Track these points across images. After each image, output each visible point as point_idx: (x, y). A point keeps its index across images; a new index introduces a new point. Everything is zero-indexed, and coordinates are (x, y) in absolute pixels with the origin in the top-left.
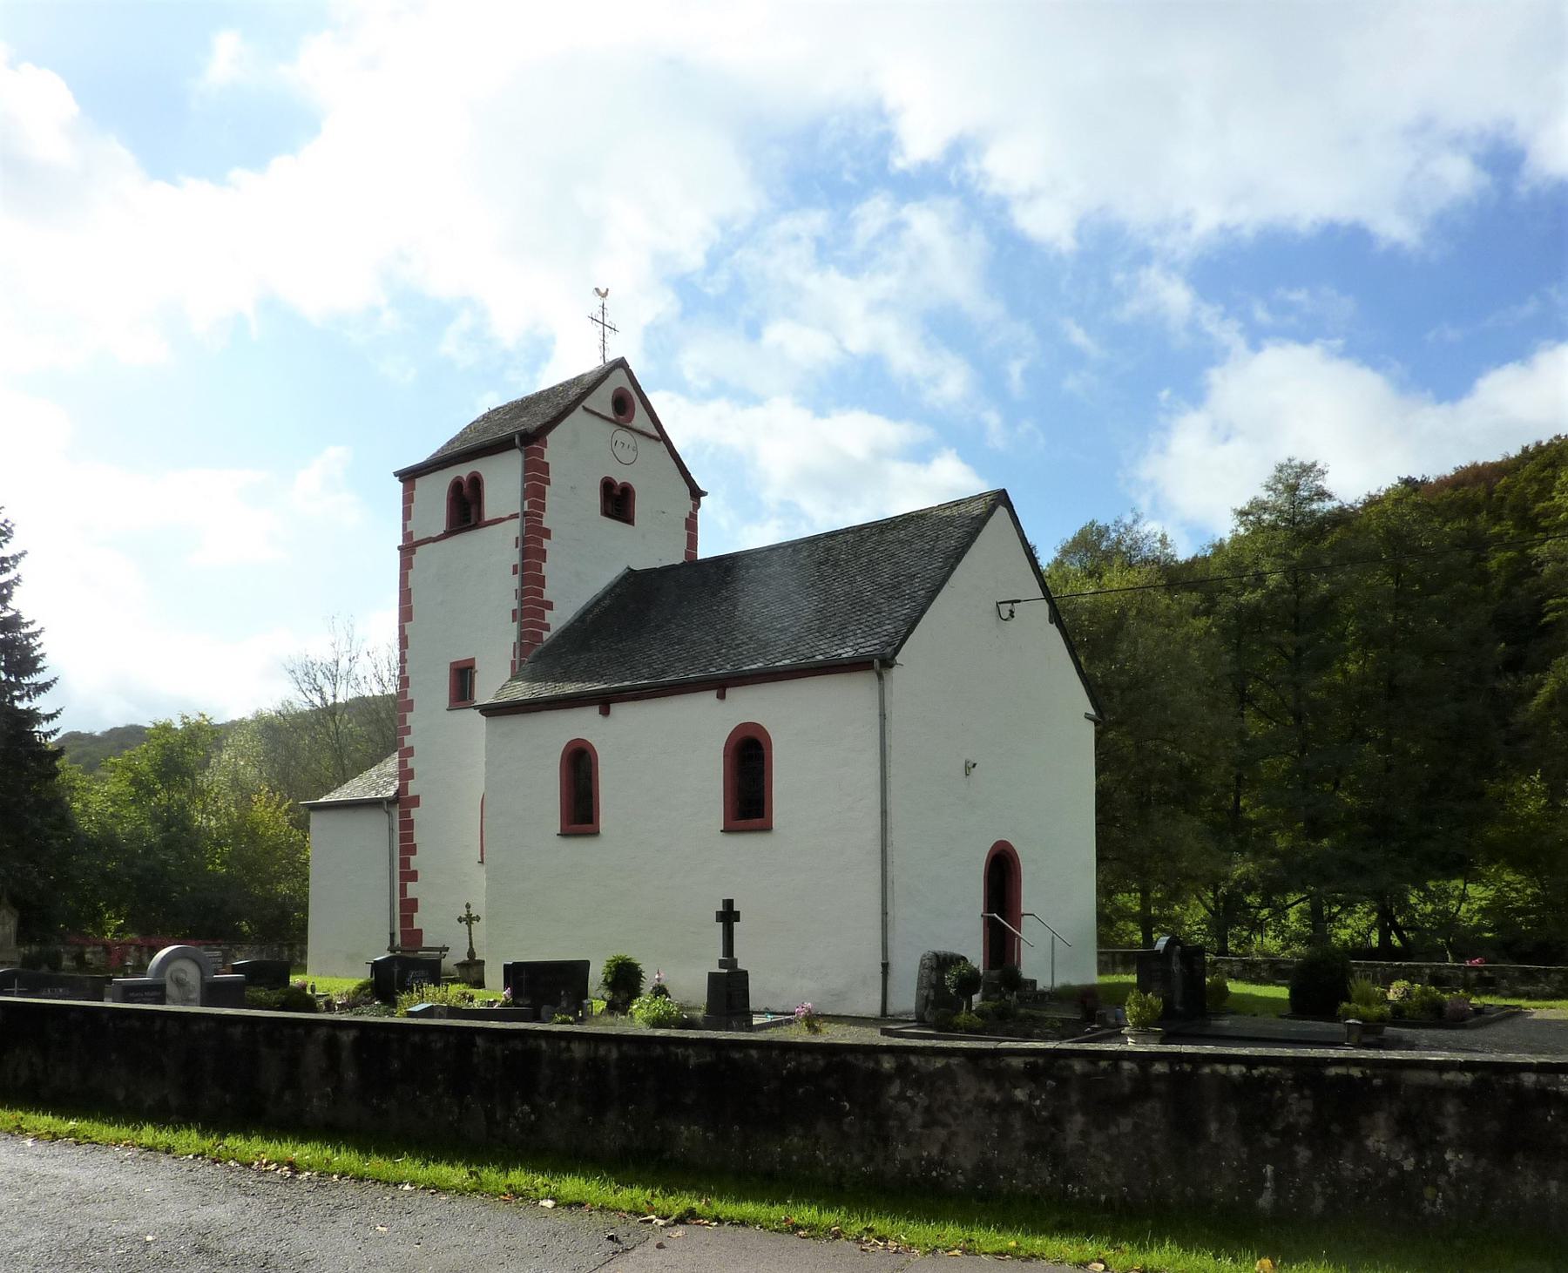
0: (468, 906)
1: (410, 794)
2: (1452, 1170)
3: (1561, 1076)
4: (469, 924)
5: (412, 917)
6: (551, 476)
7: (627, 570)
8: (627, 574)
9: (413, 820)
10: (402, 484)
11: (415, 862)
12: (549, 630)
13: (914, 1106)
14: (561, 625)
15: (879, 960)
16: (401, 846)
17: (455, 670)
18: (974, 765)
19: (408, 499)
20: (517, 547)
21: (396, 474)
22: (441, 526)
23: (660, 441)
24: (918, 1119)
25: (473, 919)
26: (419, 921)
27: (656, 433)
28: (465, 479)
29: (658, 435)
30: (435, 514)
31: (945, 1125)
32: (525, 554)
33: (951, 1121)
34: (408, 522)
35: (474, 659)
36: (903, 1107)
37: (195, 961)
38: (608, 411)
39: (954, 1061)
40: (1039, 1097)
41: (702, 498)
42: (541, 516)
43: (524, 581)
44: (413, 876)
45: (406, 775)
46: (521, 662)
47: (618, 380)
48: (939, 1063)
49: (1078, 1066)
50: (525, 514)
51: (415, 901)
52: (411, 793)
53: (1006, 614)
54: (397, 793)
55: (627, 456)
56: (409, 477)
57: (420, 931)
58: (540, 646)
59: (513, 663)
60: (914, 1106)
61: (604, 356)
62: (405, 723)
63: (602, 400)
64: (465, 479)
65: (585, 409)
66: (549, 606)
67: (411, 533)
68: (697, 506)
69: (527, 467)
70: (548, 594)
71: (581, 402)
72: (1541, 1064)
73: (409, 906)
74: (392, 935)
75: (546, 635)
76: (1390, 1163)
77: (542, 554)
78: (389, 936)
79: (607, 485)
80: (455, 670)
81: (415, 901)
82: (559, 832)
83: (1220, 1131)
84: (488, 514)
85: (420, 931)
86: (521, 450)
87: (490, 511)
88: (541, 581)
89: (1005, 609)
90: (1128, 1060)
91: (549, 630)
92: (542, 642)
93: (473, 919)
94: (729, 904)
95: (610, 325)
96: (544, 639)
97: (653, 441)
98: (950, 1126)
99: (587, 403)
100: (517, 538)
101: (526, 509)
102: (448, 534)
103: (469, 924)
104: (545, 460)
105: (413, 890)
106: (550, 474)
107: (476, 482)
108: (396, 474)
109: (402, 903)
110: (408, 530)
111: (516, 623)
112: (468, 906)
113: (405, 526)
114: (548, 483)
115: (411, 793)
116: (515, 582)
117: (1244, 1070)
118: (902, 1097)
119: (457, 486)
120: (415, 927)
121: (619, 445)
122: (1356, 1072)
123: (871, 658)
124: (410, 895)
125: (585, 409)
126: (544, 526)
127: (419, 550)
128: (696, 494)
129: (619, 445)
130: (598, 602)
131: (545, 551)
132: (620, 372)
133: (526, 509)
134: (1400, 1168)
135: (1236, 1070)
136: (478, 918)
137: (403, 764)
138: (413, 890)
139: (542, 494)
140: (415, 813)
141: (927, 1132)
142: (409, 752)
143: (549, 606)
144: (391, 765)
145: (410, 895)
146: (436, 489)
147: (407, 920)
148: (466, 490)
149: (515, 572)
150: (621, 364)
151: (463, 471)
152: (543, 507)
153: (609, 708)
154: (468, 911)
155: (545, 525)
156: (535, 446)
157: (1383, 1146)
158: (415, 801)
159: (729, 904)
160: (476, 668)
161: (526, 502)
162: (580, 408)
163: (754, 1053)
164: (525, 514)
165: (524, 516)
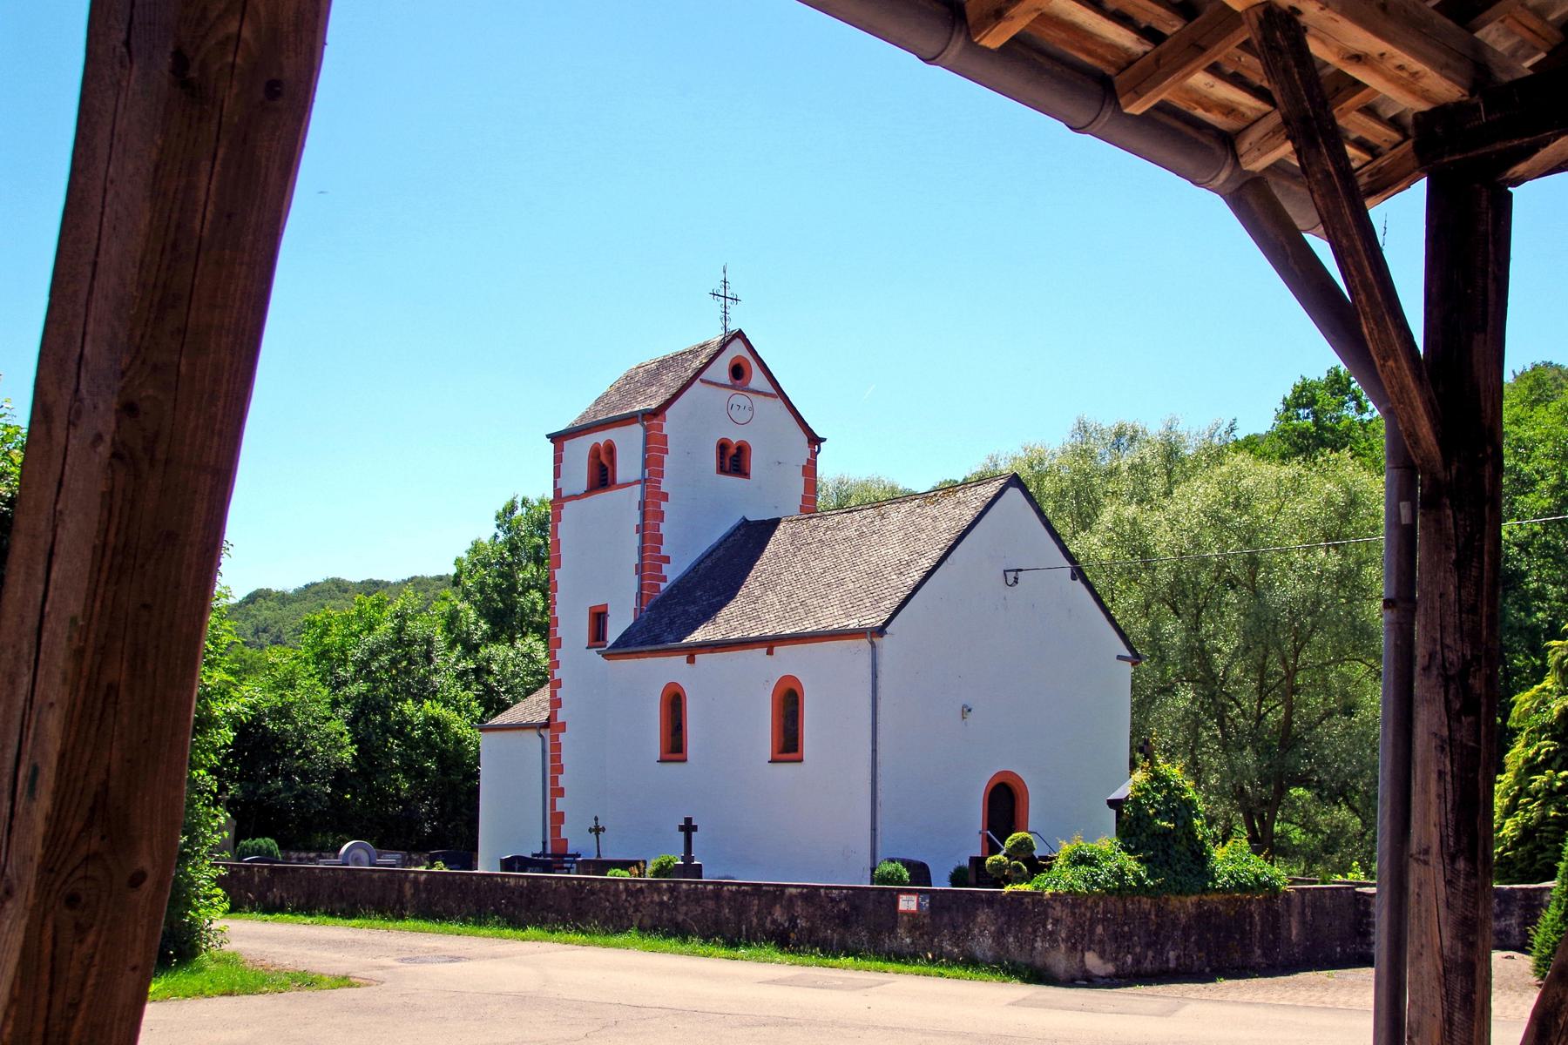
0: (596, 819)
1: (559, 720)
6: (669, 447)
8: (742, 524)
17: (594, 614)
18: (970, 710)
19: (558, 460)
21: (548, 436)
24: (632, 910)
25: (600, 830)
26: (565, 832)
27: (769, 388)
29: (774, 392)
30: (579, 477)
36: (627, 904)
37: (366, 851)
38: (725, 377)
41: (822, 444)
42: (659, 482)
44: (560, 792)
45: (556, 703)
47: (737, 349)
51: (562, 814)
53: (1011, 581)
55: (742, 416)
56: (557, 439)
63: (721, 370)
66: (667, 560)
68: (815, 455)
69: (647, 440)
70: (664, 551)
73: (559, 818)
75: (663, 586)
76: (782, 924)
77: (660, 516)
79: (723, 447)
80: (594, 614)
81: (562, 814)
84: (620, 478)
86: (643, 425)
87: (621, 477)
88: (659, 539)
89: (1011, 576)
93: (600, 830)
94: (688, 820)
96: (662, 589)
99: (704, 376)
101: (647, 476)
105: (561, 804)
107: (610, 449)
108: (548, 436)
112: (596, 819)
119: (595, 453)
124: (558, 809)
127: (567, 505)
128: (815, 440)
129: (735, 407)
130: (709, 554)
132: (738, 343)
135: (734, 888)
136: (603, 830)
137: (553, 694)
138: (561, 804)
139: (661, 463)
140: (562, 737)
142: (558, 684)
144: (545, 692)
145: (558, 809)
146: (580, 450)
147: (556, 830)
148: (603, 459)
150: (740, 335)
151: (600, 438)
152: (661, 474)
158: (563, 726)
159: (688, 820)
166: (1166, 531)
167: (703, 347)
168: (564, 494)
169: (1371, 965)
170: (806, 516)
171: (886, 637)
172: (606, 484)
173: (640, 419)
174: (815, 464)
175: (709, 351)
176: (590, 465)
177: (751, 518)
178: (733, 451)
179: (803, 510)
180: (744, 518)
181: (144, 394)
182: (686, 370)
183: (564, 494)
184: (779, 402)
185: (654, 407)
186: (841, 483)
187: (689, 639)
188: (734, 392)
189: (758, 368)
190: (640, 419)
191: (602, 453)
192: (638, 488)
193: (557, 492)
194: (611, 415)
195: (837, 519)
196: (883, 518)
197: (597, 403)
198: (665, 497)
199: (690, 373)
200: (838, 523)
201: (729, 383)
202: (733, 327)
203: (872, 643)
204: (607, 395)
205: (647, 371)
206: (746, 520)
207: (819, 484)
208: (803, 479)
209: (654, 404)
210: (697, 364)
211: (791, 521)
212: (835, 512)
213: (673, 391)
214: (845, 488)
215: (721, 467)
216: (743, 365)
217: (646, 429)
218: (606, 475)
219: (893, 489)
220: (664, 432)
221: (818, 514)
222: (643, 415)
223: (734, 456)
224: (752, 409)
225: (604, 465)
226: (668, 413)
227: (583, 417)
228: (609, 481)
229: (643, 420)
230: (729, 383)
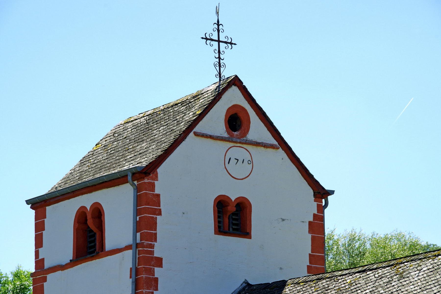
6: (163, 207)
7: (244, 285)
8: (244, 289)
10: (34, 211)
15: (45, 233)
16: (155, 230)
20: (131, 277)
21: (28, 202)
23: (278, 148)
27: (271, 140)
28: (88, 208)
29: (275, 142)
34: (40, 250)
41: (330, 198)
42: (152, 246)
50: (137, 245)
61: (220, 74)
64: (88, 209)
68: (321, 209)
69: (138, 200)
71: (193, 129)
84: (109, 245)
86: (133, 185)
95: (226, 40)
99: (197, 129)
100: (131, 269)
101: (138, 241)
102: (73, 263)
108: (28, 202)
110: (40, 257)
113: (37, 254)
114: (160, 214)
125: (196, 134)
126: (155, 255)
127: (49, 277)
129: (233, 161)
131: (156, 280)
132: (234, 90)
139: (153, 225)
148: (90, 222)
152: (154, 237)
155: (156, 255)
156: (146, 181)
161: (138, 234)
162: (192, 134)
164: (137, 245)
166: (396, 248)
167: (196, 97)
168: (47, 265)
169: (132, 249)
170: (315, 277)
172: (93, 252)
173: (130, 178)
174: (322, 219)
175: (203, 101)
176: (77, 231)
177: (252, 282)
178: (232, 209)
179: (310, 270)
180: (246, 282)
181: (146, 234)
182: (178, 124)
183: (47, 265)
184: (281, 153)
185: (144, 164)
186: (352, 239)
187: (89, 211)
188: (232, 144)
189: (257, 118)
190: (130, 178)
191: (89, 217)
192: (129, 253)
193: (39, 263)
194: (98, 176)
195: (349, 279)
196: (402, 277)
197: (82, 162)
198: (159, 262)
199: (183, 127)
200: (351, 284)
201: (226, 135)
202: (228, 73)
203: (128, 247)
204: (92, 154)
205: (136, 127)
206: (248, 285)
207: (328, 243)
208: (310, 236)
209: (144, 162)
210: (190, 116)
211: (298, 283)
212: (347, 272)
213: (165, 146)
214: (357, 245)
215: (219, 227)
216: (241, 115)
217: (138, 189)
218: (94, 241)
219: (414, 245)
220: (157, 192)
221: (328, 275)
222: (133, 174)
223: (233, 214)
224: (251, 162)
225: (91, 231)
226: (160, 170)
227: (66, 179)
228: (97, 247)
229: (133, 180)
230: (226, 135)
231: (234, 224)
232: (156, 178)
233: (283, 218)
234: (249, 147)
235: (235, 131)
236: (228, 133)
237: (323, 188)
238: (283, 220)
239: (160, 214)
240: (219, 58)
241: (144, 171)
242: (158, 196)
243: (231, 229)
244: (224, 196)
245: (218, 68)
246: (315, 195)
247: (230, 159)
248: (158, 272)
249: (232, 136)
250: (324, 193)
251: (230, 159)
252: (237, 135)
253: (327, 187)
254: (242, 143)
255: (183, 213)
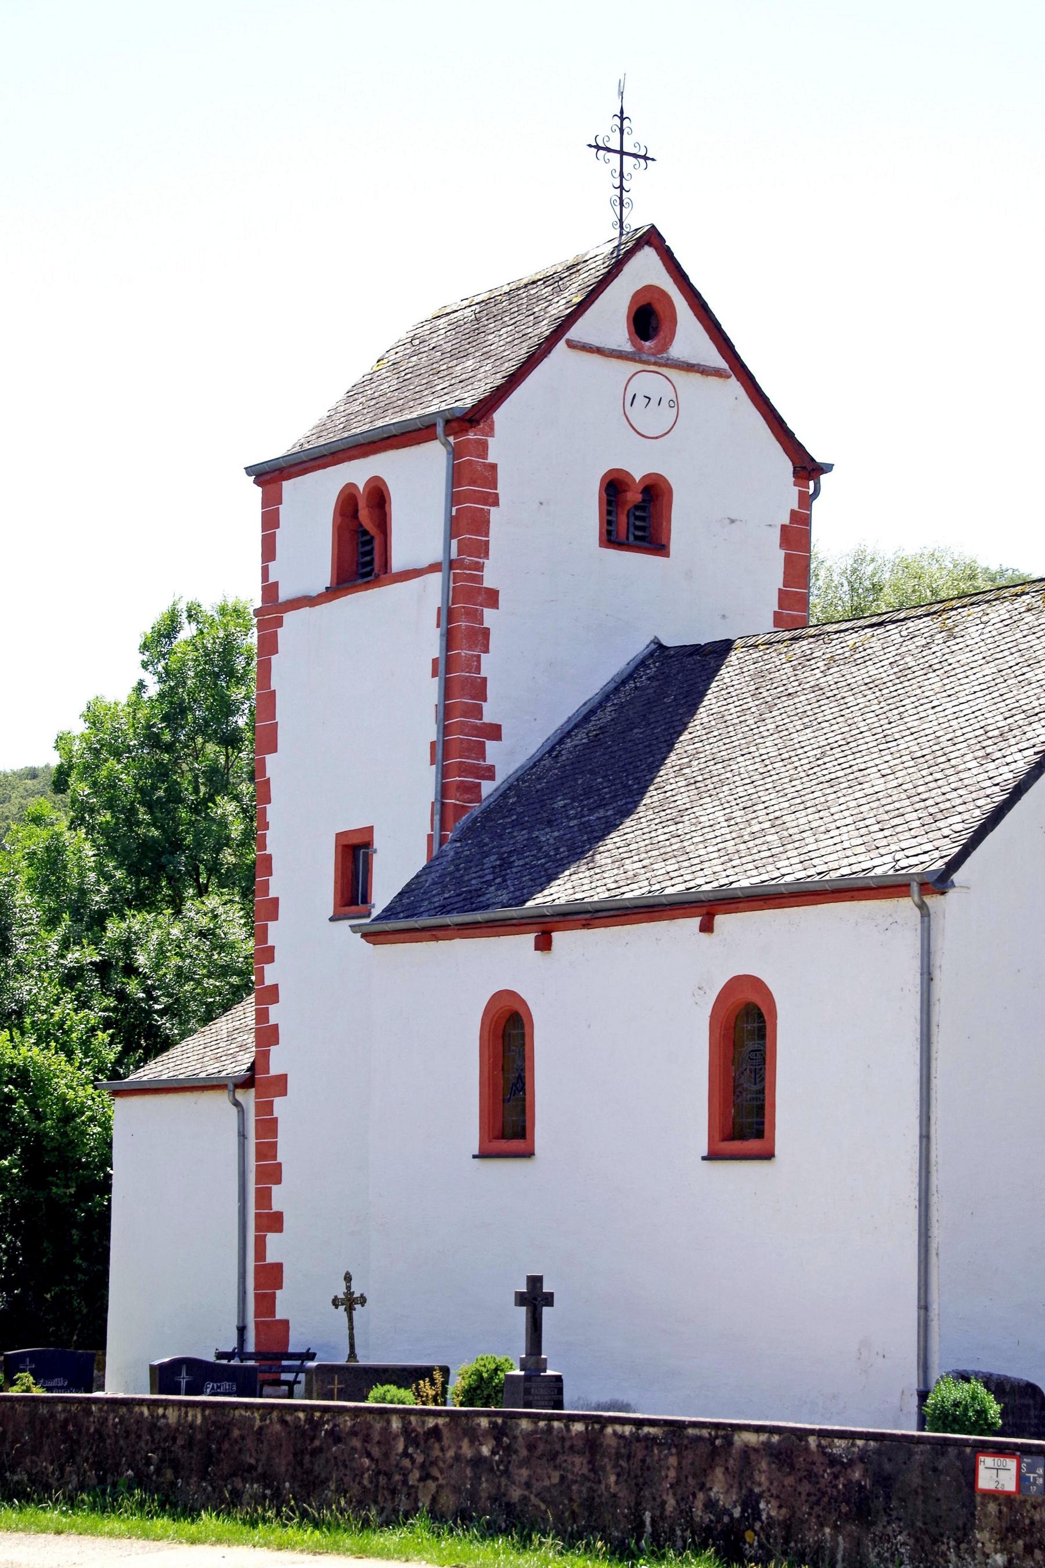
0: (348, 1278)
2: (764, 1517)
3: (836, 1440)
4: (349, 1293)
5: (273, 1297)
6: (500, 490)
7: (653, 646)
9: (280, 1164)
10: (260, 489)
11: (280, 1198)
12: (492, 777)
13: (413, 1461)
14: (517, 765)
20: (438, 626)
21: (249, 470)
22: (322, 577)
23: (729, 377)
24: (416, 1474)
31: (435, 1479)
32: (449, 639)
33: (438, 1475)
34: (271, 564)
35: (370, 829)
38: (620, 336)
39: (441, 1421)
40: (498, 1453)
42: (480, 567)
43: (447, 690)
46: (443, 840)
48: (431, 1422)
49: (525, 1424)
50: (452, 564)
51: (279, 1267)
52: (275, 1070)
54: (252, 1068)
57: (286, 1323)
58: (476, 808)
59: (430, 837)
60: (413, 1461)
62: (266, 942)
65: (571, 345)
66: (494, 732)
67: (276, 585)
69: (457, 475)
70: (490, 713)
71: (564, 334)
72: (821, 1430)
74: (242, 1330)
75: (487, 788)
77: (481, 638)
78: (236, 1332)
82: (476, 1152)
83: (617, 1483)
84: (398, 561)
85: (286, 1323)
87: (400, 558)
88: (479, 689)
90: (558, 1420)
91: (492, 777)
92: (478, 799)
94: (535, 1281)
97: (713, 380)
98: (437, 1479)
99: (574, 333)
101: (454, 555)
102: (333, 592)
103: (349, 1293)
104: (491, 459)
105: (276, 1247)
106: (499, 486)
108: (249, 470)
109: (257, 1269)
110: (271, 580)
111: (434, 766)
112: (348, 1278)
114: (496, 503)
115: (275, 1070)
116: (431, 690)
117: (634, 1430)
118: (405, 1454)
120: (278, 1317)
121: (640, 401)
122: (705, 1433)
123: (904, 881)
125: (571, 345)
129: (640, 401)
131: (486, 632)
132: (648, 256)
133: (454, 555)
134: (731, 1515)
135: (628, 1430)
137: (262, 1015)
138: (276, 1247)
139: (482, 524)
140: (280, 1105)
141: (421, 1484)
142: (271, 994)
143: (494, 732)
147: (266, 1303)
149: (435, 674)
152: (483, 550)
153: (550, 937)
154: (349, 1288)
155: (487, 583)
157: (722, 1497)
159: (535, 1281)
160: (376, 844)
161: (454, 543)
162: (562, 344)
163: (301, 1415)
164: (452, 564)
165: (451, 568)
171: (952, 894)
184: (734, 386)
188: (639, 367)
201: (628, 347)
208: (782, 554)
224: (674, 403)
226: (500, 416)
230: (628, 347)
231: (637, 528)
232: (490, 431)
233: (733, 517)
234: (672, 373)
235: (646, 340)
236: (633, 344)
237: (813, 460)
238: (732, 521)
239: (496, 503)
240: (621, 187)
241: (468, 417)
242: (494, 467)
243: (631, 538)
244: (628, 474)
245: (618, 209)
246: (796, 474)
247: (635, 396)
248: (490, 617)
249: (640, 349)
250: (813, 470)
251: (635, 396)
252: (650, 348)
253: (819, 458)
254: (660, 365)
255: (541, 504)
